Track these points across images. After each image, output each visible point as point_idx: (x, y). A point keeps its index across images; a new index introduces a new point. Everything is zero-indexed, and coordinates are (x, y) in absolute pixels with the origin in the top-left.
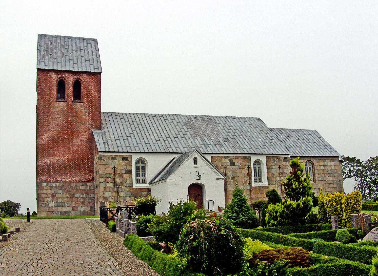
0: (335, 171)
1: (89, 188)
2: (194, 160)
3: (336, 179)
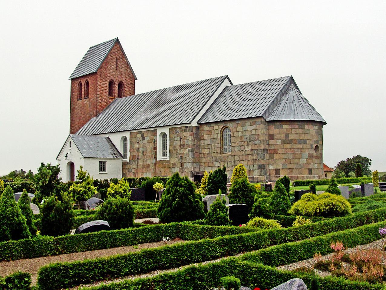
0: (256, 137)
3: (257, 148)
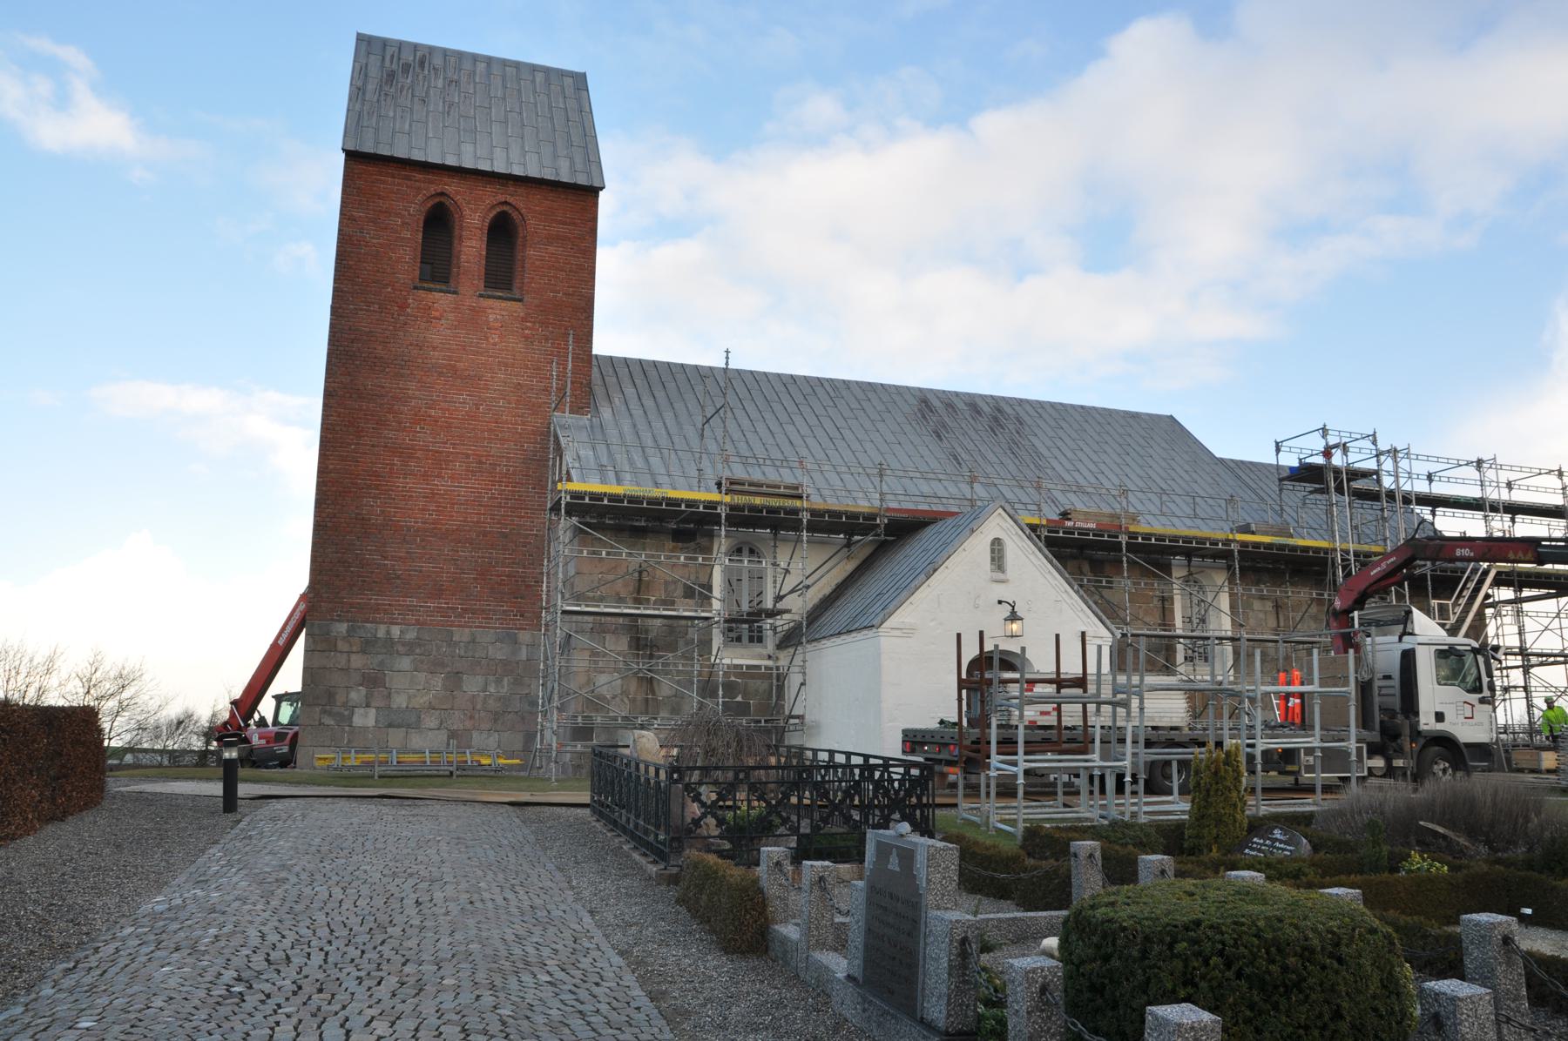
1: (523, 655)
2: (993, 551)
